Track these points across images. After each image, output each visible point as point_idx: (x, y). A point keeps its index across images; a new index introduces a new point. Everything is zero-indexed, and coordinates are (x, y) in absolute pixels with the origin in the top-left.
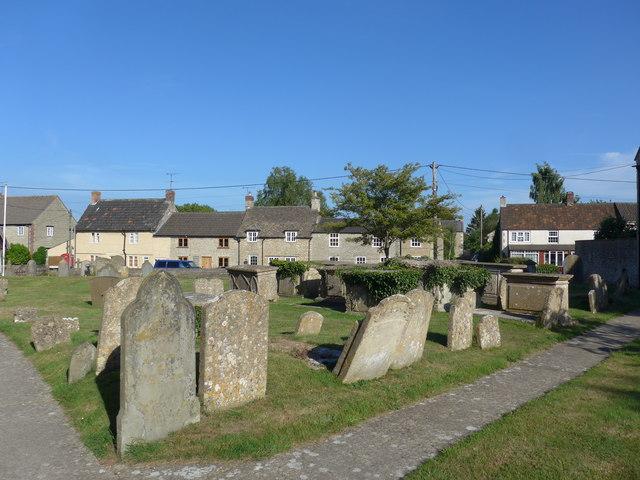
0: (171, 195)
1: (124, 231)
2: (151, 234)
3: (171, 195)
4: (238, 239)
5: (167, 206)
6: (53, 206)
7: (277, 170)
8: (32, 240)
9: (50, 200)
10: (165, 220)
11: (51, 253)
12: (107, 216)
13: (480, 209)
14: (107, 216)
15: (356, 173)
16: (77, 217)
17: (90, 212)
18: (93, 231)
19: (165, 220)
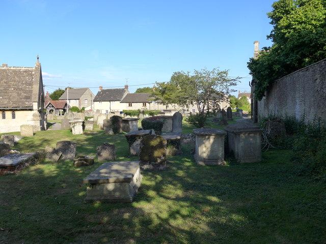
0: (127, 87)
1: (110, 101)
2: (119, 102)
3: (127, 87)
4: (149, 103)
5: (125, 91)
6: (87, 91)
7: (176, 73)
8: (80, 105)
9: (86, 89)
10: (124, 96)
11: (85, 109)
12: (107, 95)
13: (270, 23)
14: (107, 95)
15: (157, 84)
16: (95, 93)
17: (99, 94)
18: (100, 101)
19: (124, 96)
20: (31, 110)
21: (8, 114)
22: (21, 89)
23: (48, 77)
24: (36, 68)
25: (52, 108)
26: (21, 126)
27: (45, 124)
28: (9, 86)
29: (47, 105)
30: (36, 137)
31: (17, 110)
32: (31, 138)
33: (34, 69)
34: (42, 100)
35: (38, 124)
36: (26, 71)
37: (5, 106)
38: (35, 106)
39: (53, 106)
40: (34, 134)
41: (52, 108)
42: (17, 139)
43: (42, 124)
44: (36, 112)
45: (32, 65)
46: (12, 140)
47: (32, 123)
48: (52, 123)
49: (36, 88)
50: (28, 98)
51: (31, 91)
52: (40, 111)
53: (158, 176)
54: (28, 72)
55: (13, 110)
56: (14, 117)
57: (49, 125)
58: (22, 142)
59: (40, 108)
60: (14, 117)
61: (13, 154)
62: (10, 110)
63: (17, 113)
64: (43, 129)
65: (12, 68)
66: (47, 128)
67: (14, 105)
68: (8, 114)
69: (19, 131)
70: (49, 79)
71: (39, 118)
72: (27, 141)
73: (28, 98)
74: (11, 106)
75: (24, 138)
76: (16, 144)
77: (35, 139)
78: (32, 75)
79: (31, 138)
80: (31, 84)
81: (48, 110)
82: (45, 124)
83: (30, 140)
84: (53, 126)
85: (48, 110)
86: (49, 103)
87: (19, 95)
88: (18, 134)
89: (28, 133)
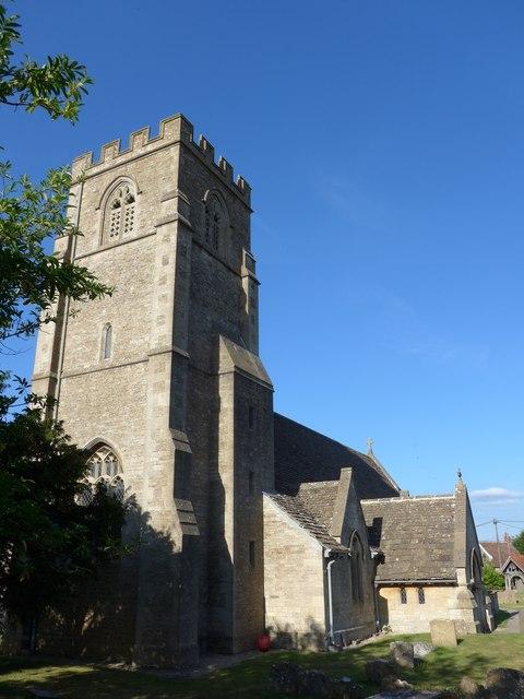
20: (454, 585)
21: (412, 593)
22: (433, 542)
23: (508, 497)
24: (457, 495)
25: (516, 573)
26: (432, 623)
27: (489, 617)
28: (411, 537)
29: (506, 565)
30: (462, 648)
31: (426, 585)
32: (450, 652)
33: (454, 497)
34: (475, 563)
35: (469, 617)
36: (439, 504)
37: (402, 577)
38: (461, 577)
39: (518, 569)
40: (459, 641)
41: (516, 573)
42: (421, 651)
43: (479, 615)
44: (462, 589)
45: (446, 490)
46: (409, 654)
47: (456, 615)
48: (510, 612)
49: (460, 538)
50: (446, 559)
51: (450, 545)
52: (473, 588)
53: (134, 664)
54: (443, 505)
55: (420, 586)
56: (422, 600)
57: (501, 617)
58: (431, 659)
59: (472, 581)
60: (422, 600)
61: (401, 688)
62: (414, 585)
63: (428, 592)
64: (483, 628)
65: (414, 500)
66: (495, 627)
67: (421, 575)
68: (412, 593)
69: (429, 631)
70: (511, 501)
71: (470, 604)
72: (442, 657)
73: (446, 559)
74: (416, 576)
75: (438, 650)
76: (418, 662)
77: (460, 653)
78: (451, 510)
79: (450, 652)
80: (450, 529)
81: (508, 579)
82: (489, 617)
83: (450, 655)
84: (510, 620)
85: (508, 579)
86: (507, 562)
87: (429, 552)
88: (425, 638)
89: (446, 638)
